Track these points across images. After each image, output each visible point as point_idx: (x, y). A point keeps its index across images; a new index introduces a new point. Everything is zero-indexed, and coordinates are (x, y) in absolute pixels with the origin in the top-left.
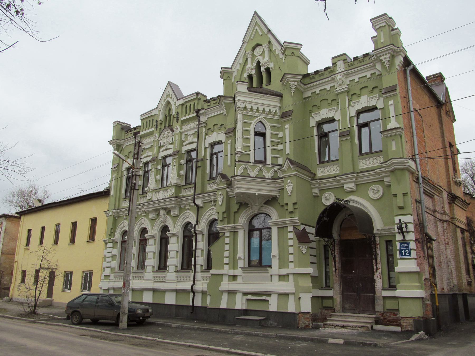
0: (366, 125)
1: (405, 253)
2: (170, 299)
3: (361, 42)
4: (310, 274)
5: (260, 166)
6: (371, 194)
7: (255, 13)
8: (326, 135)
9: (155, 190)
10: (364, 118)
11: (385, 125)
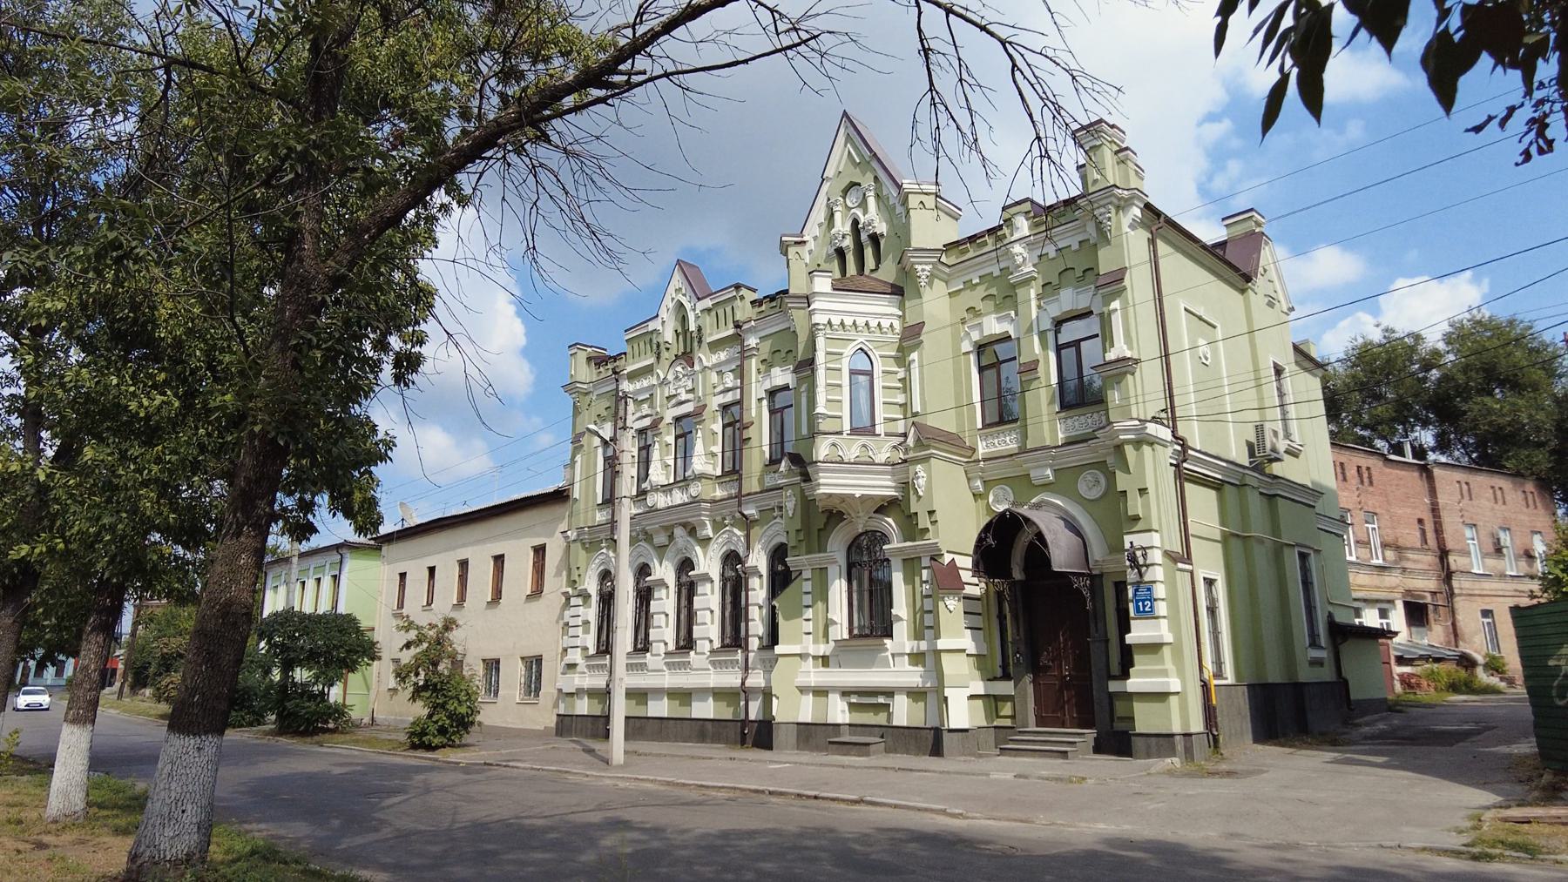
0: (1076, 344)
2: (705, 709)
5: (864, 440)
6: (1082, 488)
7: (845, 114)
9: (666, 489)
10: (1070, 332)
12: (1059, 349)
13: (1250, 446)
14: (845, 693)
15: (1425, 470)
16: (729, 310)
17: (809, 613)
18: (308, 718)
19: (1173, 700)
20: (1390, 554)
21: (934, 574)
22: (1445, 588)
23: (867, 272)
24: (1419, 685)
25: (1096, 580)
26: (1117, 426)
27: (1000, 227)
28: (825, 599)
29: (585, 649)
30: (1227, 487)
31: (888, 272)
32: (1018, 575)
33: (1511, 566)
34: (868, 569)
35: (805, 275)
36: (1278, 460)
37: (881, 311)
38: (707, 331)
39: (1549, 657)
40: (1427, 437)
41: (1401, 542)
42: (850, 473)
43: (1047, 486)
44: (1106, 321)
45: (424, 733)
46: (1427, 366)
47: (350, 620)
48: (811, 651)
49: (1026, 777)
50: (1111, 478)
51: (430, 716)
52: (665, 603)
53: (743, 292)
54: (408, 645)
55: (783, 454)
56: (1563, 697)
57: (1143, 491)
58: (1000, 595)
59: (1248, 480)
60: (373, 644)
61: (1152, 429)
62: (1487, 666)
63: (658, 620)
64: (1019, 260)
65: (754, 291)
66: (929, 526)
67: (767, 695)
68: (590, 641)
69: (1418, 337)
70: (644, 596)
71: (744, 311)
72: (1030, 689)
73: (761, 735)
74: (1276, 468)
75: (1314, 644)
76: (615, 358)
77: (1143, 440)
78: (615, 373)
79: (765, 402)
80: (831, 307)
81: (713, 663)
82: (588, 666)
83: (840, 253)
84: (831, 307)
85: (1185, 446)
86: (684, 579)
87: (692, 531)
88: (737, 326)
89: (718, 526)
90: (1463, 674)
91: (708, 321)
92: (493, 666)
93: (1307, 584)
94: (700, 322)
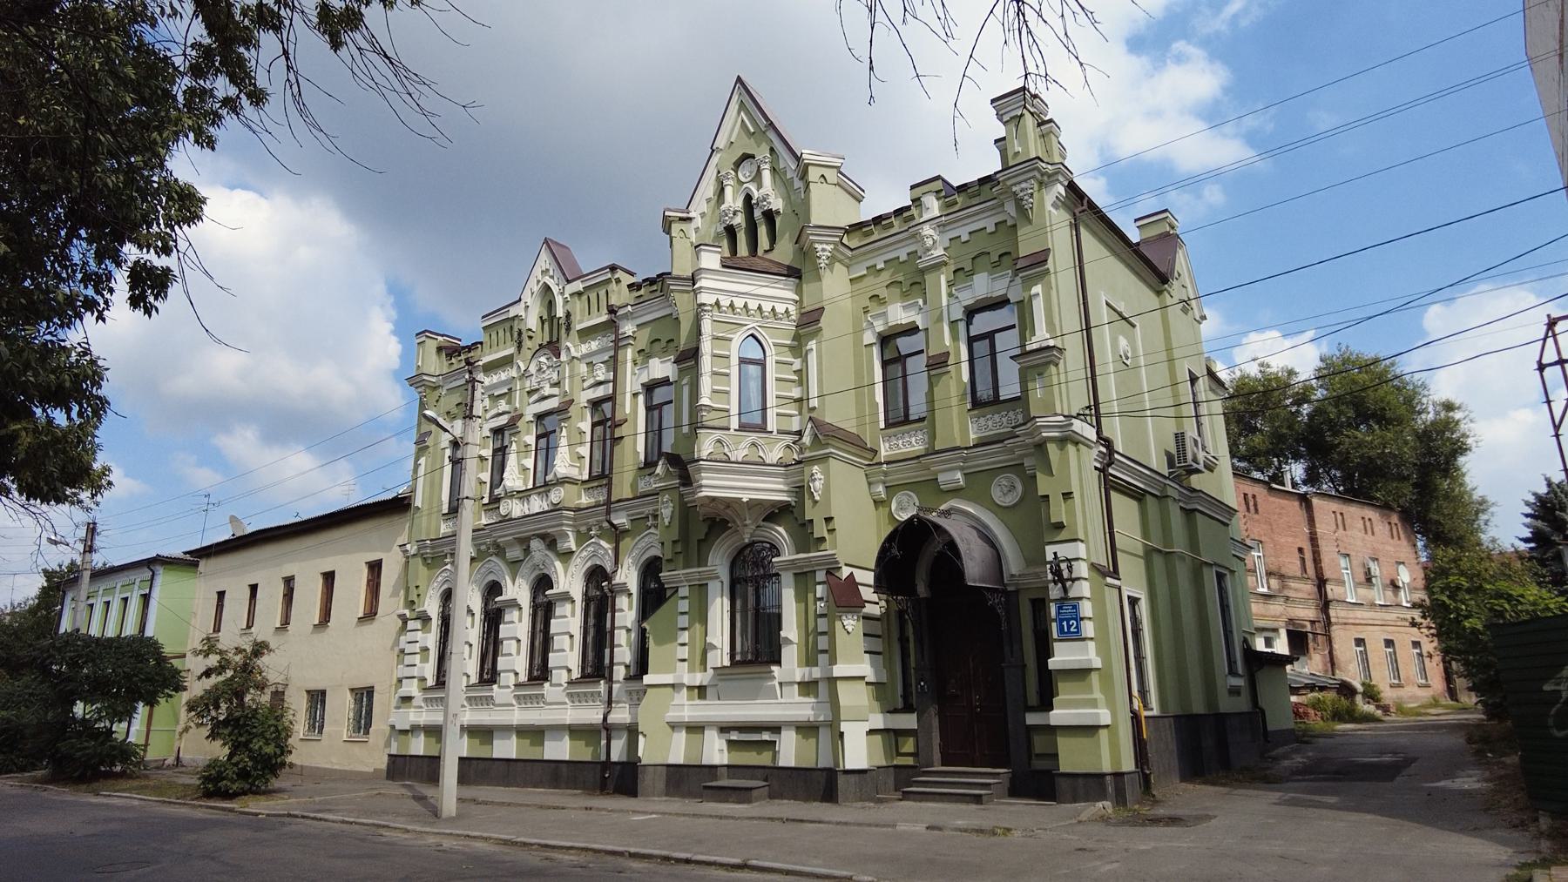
0: (990, 336)
1: (1069, 627)
2: (559, 749)
3: (42, 582)
4: (863, 678)
5: (753, 436)
6: (997, 494)
7: (739, 80)
8: (901, 359)
9: (523, 495)
10: (982, 323)
11: (1023, 339)
12: (971, 341)
13: (1169, 455)
14: (724, 729)
15: (1304, 499)
16: (602, 293)
17: (685, 637)
18: (98, 763)
19: (1103, 733)
20: (1274, 582)
21: (831, 589)
22: (1322, 617)
23: (760, 252)
24: (1306, 714)
25: (1010, 597)
26: (1040, 422)
27: (908, 208)
28: (704, 620)
29: (423, 679)
30: (1148, 497)
31: (784, 252)
32: (922, 590)
33: (1379, 595)
34: (751, 577)
35: (690, 251)
36: (1198, 471)
37: (778, 295)
38: (576, 318)
39: (1546, 680)
40: (1296, 470)
41: (1283, 571)
42: (737, 474)
43: (956, 492)
44: (1024, 308)
45: (220, 777)
46: (1302, 398)
47: (153, 646)
48: (686, 681)
49: (940, 829)
50: (1030, 481)
51: (231, 756)
52: (517, 627)
53: (619, 274)
54: (207, 673)
55: (660, 454)
56: (1560, 728)
57: (1067, 496)
58: (901, 614)
59: (1170, 492)
60: (176, 672)
61: (1078, 425)
62: (1364, 694)
63: (508, 646)
64: (929, 242)
65: (632, 274)
66: (826, 535)
67: (633, 731)
68: (429, 671)
69: (1291, 373)
70: (493, 618)
71: (620, 295)
72: (936, 722)
73: (622, 779)
74: (1195, 481)
75: (1233, 672)
76: (469, 348)
77: (1068, 439)
78: (468, 363)
79: (641, 398)
80: (720, 286)
81: (570, 695)
82: (426, 700)
83: (731, 232)
84: (720, 286)
85: (1108, 443)
86: (541, 599)
87: (551, 542)
88: (612, 310)
89: (582, 538)
90: (1344, 702)
91: (578, 306)
92: (317, 698)
93: (1225, 608)
94: (568, 307)
